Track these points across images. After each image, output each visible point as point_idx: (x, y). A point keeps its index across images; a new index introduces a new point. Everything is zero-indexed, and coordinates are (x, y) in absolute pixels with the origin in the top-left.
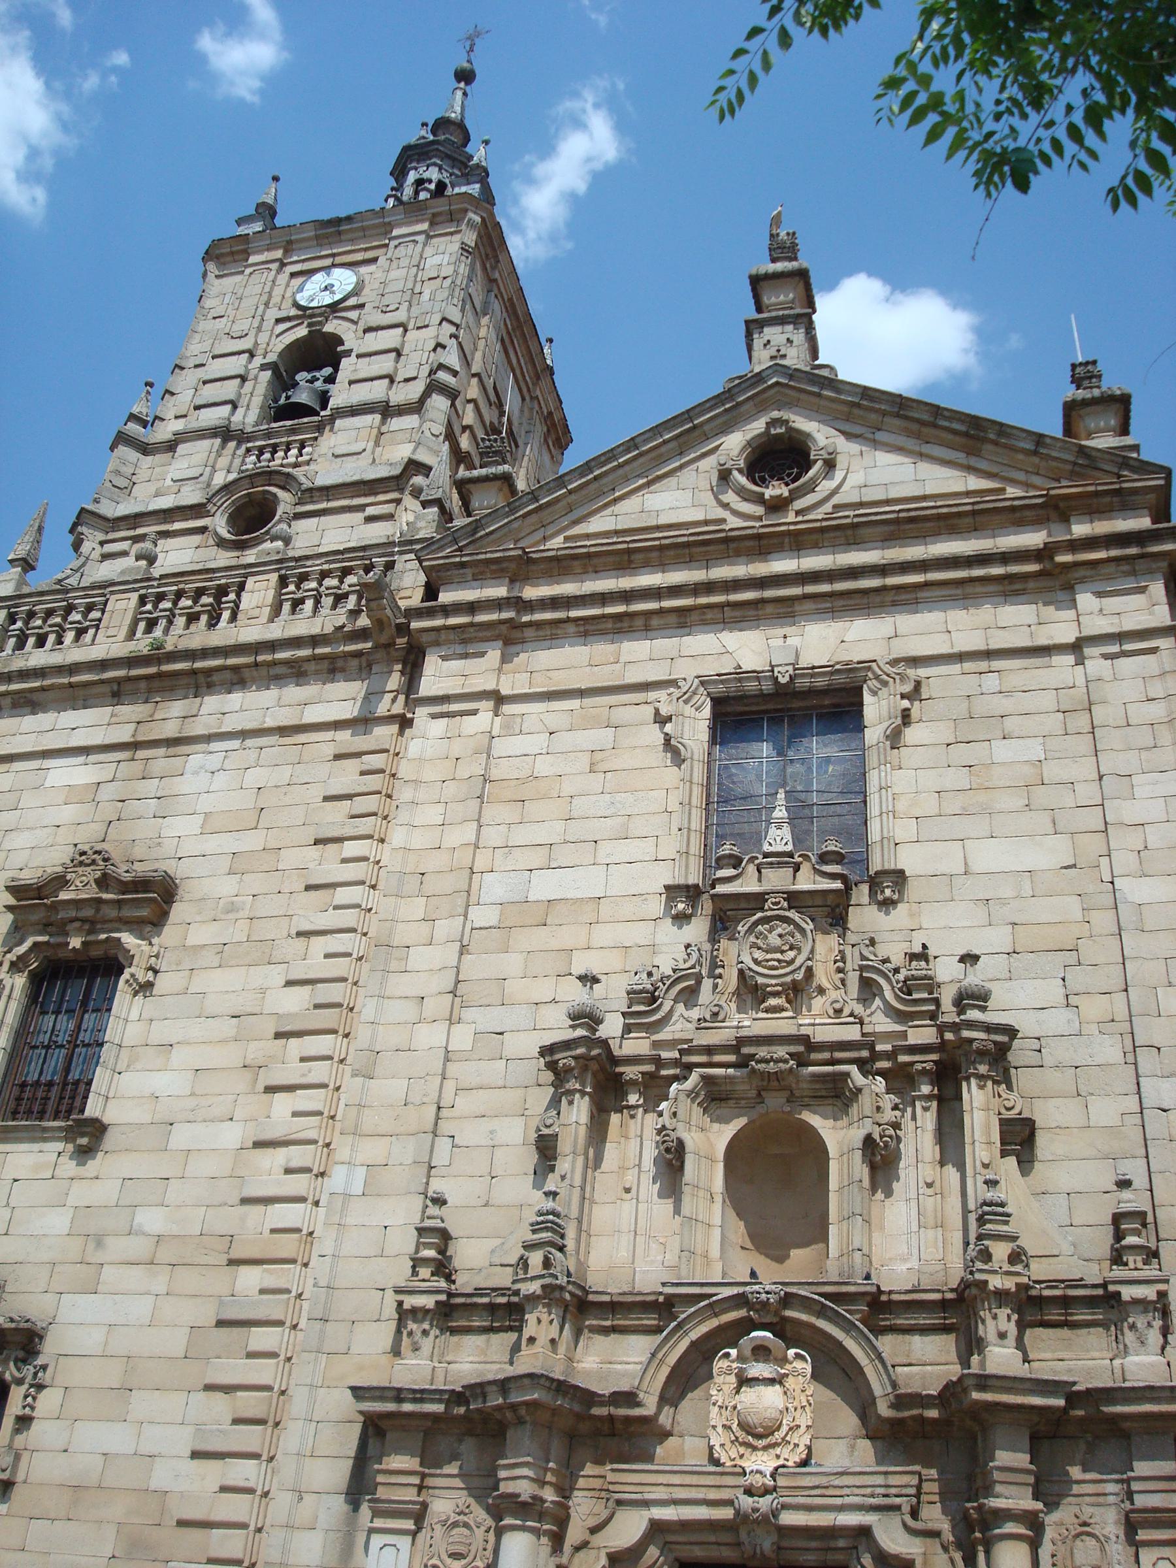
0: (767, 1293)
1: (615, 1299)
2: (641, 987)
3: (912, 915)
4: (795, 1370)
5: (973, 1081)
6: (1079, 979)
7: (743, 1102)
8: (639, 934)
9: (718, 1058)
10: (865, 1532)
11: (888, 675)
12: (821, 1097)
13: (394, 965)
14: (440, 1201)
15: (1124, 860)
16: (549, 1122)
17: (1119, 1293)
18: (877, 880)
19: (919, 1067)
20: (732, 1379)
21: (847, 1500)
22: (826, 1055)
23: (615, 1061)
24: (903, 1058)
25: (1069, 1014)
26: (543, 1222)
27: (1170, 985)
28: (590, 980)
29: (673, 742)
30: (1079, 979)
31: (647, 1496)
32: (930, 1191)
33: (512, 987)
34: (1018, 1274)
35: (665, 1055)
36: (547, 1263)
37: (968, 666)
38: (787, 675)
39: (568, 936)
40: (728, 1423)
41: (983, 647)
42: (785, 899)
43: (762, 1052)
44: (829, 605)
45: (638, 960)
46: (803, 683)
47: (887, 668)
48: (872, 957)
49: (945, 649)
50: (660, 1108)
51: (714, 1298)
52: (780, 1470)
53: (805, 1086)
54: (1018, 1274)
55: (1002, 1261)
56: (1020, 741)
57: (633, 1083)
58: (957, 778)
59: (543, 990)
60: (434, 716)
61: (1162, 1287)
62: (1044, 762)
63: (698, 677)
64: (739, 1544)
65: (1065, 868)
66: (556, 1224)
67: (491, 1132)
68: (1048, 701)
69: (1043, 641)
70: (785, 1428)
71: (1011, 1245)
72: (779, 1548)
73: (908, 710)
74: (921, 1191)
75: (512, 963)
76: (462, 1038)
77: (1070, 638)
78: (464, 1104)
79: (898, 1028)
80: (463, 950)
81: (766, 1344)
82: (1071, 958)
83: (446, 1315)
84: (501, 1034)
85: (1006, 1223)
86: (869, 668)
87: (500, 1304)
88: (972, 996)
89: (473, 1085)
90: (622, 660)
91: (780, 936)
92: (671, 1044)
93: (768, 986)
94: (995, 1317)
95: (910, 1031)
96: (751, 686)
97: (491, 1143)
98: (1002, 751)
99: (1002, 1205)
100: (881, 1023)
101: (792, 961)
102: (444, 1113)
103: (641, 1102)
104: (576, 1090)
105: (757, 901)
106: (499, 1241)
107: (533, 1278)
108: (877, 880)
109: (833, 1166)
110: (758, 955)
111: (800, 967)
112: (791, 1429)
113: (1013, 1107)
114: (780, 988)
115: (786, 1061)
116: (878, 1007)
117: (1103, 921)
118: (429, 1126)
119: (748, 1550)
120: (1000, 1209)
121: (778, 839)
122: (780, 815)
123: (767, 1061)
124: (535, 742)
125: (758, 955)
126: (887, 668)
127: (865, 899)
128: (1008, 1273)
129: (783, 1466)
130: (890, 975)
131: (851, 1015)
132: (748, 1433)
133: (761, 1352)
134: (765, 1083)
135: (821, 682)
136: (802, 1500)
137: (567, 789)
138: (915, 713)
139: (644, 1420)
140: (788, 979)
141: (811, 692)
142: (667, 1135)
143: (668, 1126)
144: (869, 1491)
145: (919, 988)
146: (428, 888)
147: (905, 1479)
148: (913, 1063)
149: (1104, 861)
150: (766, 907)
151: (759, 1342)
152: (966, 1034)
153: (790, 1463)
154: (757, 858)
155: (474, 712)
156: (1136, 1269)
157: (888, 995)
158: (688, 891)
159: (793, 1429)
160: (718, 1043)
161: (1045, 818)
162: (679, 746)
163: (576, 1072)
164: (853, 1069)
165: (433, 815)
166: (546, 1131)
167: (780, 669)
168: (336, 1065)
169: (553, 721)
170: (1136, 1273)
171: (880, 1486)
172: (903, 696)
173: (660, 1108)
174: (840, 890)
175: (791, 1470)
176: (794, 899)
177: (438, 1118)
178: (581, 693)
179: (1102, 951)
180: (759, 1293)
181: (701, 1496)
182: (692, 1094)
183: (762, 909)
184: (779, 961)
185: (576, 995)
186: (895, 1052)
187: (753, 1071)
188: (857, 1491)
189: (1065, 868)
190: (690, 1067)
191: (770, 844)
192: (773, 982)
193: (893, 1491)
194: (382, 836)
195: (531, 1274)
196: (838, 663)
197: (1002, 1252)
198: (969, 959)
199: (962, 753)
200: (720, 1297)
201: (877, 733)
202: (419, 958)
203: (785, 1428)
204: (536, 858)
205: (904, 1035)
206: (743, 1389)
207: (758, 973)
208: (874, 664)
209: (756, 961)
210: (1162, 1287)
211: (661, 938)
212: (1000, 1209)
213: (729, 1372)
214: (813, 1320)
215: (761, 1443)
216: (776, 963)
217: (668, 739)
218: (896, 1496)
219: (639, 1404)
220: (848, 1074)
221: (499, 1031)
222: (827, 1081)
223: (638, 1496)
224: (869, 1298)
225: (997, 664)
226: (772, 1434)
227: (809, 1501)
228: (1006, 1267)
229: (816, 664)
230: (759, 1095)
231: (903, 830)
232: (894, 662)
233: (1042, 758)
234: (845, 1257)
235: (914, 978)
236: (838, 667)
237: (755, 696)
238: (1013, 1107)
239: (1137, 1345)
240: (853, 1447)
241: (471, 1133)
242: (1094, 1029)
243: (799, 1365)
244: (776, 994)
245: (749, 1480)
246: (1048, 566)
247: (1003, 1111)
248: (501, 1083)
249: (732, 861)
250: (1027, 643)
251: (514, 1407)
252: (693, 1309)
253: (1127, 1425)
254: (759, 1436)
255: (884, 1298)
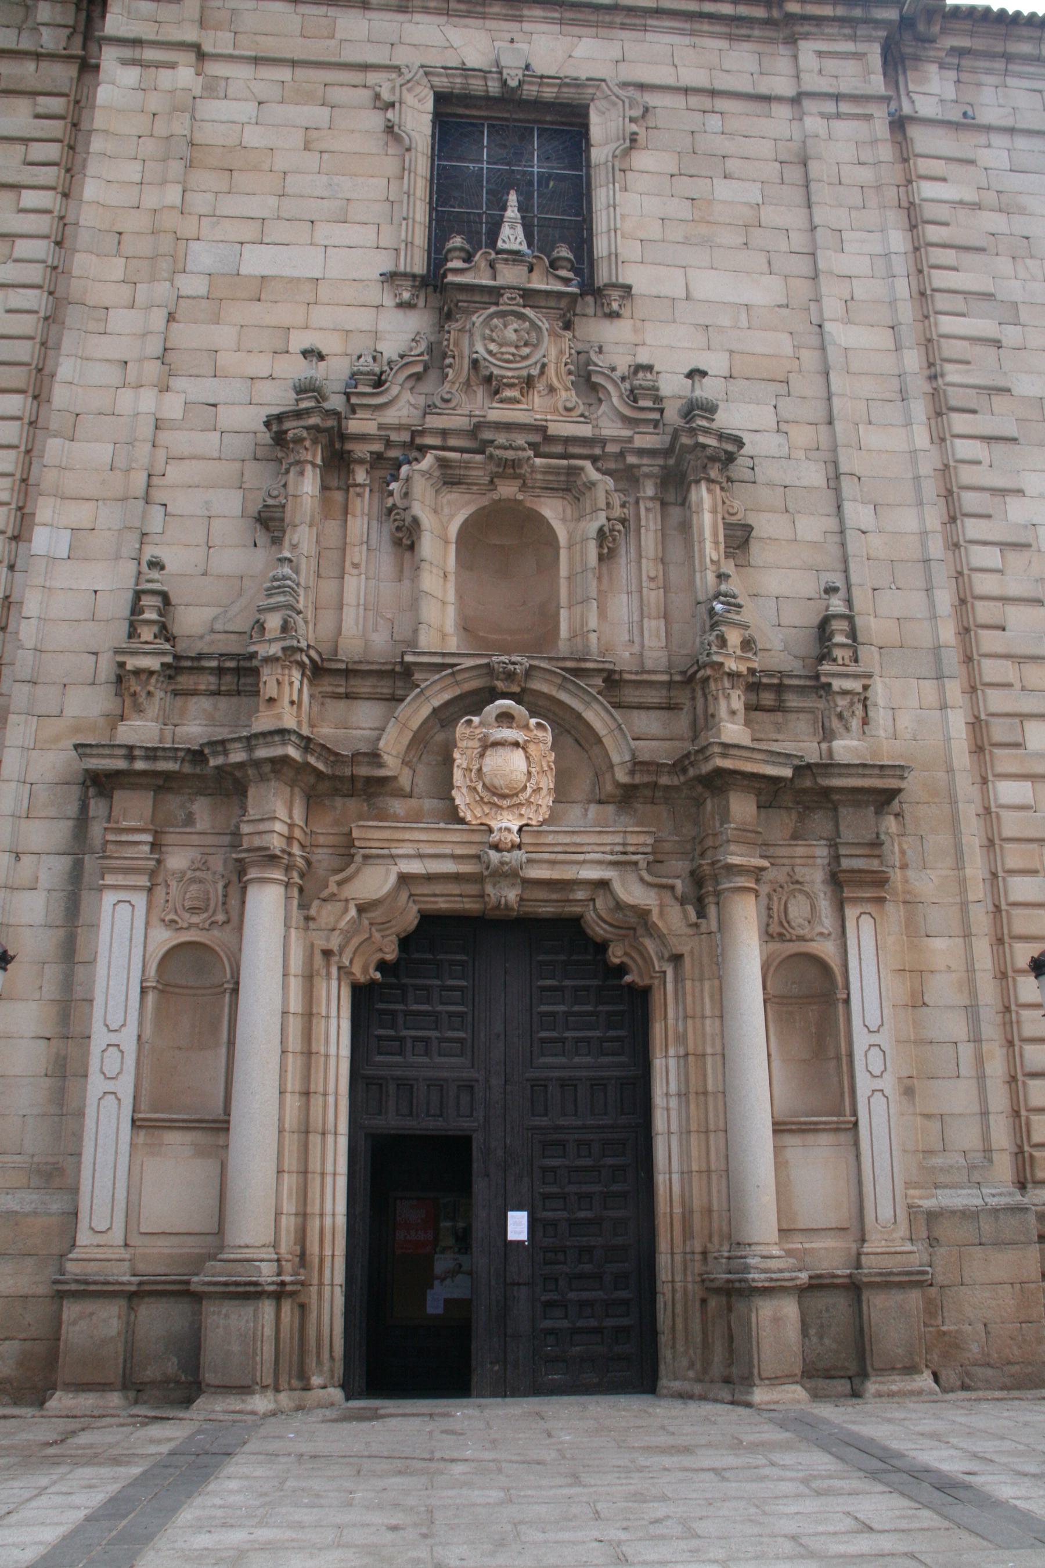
0: (514, 663)
1: (350, 667)
2: (368, 369)
3: (635, 331)
4: (536, 737)
5: (703, 486)
6: (789, 408)
7: (475, 488)
8: (363, 319)
9: (452, 442)
10: (603, 884)
11: (617, 97)
12: (551, 489)
13: (92, 326)
14: (156, 564)
15: (832, 306)
16: (275, 493)
17: (830, 685)
18: (605, 292)
19: (645, 469)
20: (476, 744)
21: (589, 857)
22: (559, 449)
23: (343, 437)
24: (631, 459)
25: (780, 439)
26: (279, 587)
27: (870, 423)
28: (313, 354)
29: (396, 129)
30: (789, 408)
31: (394, 851)
32: (653, 585)
33: (224, 359)
34: (749, 659)
35: (394, 437)
36: (285, 628)
37: (694, 101)
38: (517, 79)
39: (284, 313)
40: (473, 785)
41: (708, 86)
42: (520, 296)
43: (501, 439)
44: (557, 15)
45: (361, 344)
46: (530, 91)
47: (616, 89)
48: (601, 364)
49: (671, 81)
50: (391, 488)
51: (458, 667)
52: (525, 828)
53: (539, 476)
54: (749, 659)
55: (735, 647)
56: (740, 183)
57: (361, 462)
58: (681, 209)
59: (260, 365)
60: (125, 62)
61: (866, 681)
62: (762, 207)
63: (422, 66)
64: (482, 896)
65: (779, 306)
66: (293, 589)
67: (206, 502)
68: (766, 148)
69: (763, 90)
70: (529, 790)
71: (742, 631)
72: (522, 899)
73: (636, 134)
74: (644, 584)
75: (223, 335)
76: (173, 407)
77: (790, 92)
78: (175, 473)
79: (627, 433)
80: (171, 318)
81: (512, 712)
82: (782, 389)
83: (170, 677)
84: (215, 405)
85: (738, 613)
86: (598, 87)
87: (229, 669)
88: (701, 408)
89: (186, 454)
90: (338, 36)
91: (516, 331)
92: (399, 428)
93: (503, 377)
94: (728, 697)
95: (637, 437)
96: (476, 85)
97: (208, 514)
98: (724, 189)
99: (734, 597)
100: (611, 429)
101: (525, 358)
102: (155, 481)
103: (367, 482)
104: (307, 462)
105: (494, 293)
106: (219, 610)
107: (270, 641)
108: (605, 292)
109: (563, 554)
110: (493, 347)
111: (536, 363)
112: (534, 791)
113: (736, 514)
114: (516, 381)
115: (524, 449)
116: (604, 413)
117: (810, 358)
118: (140, 491)
119: (493, 900)
120: (732, 600)
121: (512, 238)
122: (512, 215)
123: (505, 448)
124: (247, 110)
125: (493, 347)
126: (616, 89)
127: (590, 311)
128: (741, 658)
129: (527, 825)
130: (619, 382)
131: (582, 415)
132: (494, 794)
133: (505, 718)
134: (501, 470)
135: (549, 93)
136: (546, 856)
137: (280, 164)
138: (641, 138)
139: (383, 781)
140: (524, 373)
141: (538, 104)
142: (398, 514)
143: (399, 504)
144: (608, 849)
145: (645, 397)
146: (128, 248)
147: (641, 839)
148: (639, 466)
149: (813, 306)
150: (501, 301)
151: (504, 710)
152: (702, 439)
153: (534, 823)
154: (490, 254)
155: (172, 66)
156: (844, 665)
157: (615, 400)
158: (414, 281)
159: (538, 790)
160: (453, 427)
161: (762, 258)
162: (404, 135)
163: (307, 443)
164: (587, 464)
165: (132, 172)
166: (270, 502)
167: (509, 71)
168: (26, 427)
169: (261, 89)
170: (845, 668)
171: (619, 844)
172: (632, 120)
173: (391, 488)
174: (575, 294)
175: (535, 829)
176: (528, 296)
177: (149, 486)
178: (294, 63)
179: (807, 385)
180: (504, 663)
181: (448, 851)
182: (426, 474)
183: (497, 304)
184: (513, 355)
185: (301, 370)
186: (622, 455)
187: (491, 457)
188: (597, 848)
189: (779, 306)
190: (423, 449)
191: (504, 241)
192: (510, 374)
193: (631, 849)
194: (67, 191)
195: (267, 636)
196: (566, 77)
197: (734, 638)
198: (695, 374)
199: (684, 185)
200: (463, 667)
201: (605, 152)
202: (121, 320)
203: (529, 790)
204: (249, 231)
205: (630, 440)
206: (488, 753)
207: (495, 365)
208: (603, 84)
209: (490, 352)
210: (866, 681)
211: (383, 325)
212: (732, 600)
213: (471, 737)
214: (554, 692)
215: (505, 803)
216: (511, 357)
217: (389, 129)
218: (633, 853)
219: (381, 765)
220: (582, 469)
221: (212, 402)
222: (559, 474)
223: (385, 852)
224: (605, 675)
225: (721, 104)
226: (517, 795)
227: (553, 856)
228: (739, 652)
229: (545, 74)
230: (492, 482)
231: (629, 250)
232: (625, 85)
233: (760, 201)
234: (579, 639)
235: (641, 387)
236: (567, 80)
237: (480, 98)
238: (736, 514)
239: (842, 730)
240: (586, 810)
241: (182, 503)
242: (801, 454)
243: (540, 734)
244: (511, 386)
245: (495, 838)
246: (776, 14)
247: (727, 516)
248: (216, 454)
249: (463, 255)
250: (748, 89)
251: (257, 763)
252: (437, 677)
253: (836, 797)
254: (504, 796)
255: (617, 677)
